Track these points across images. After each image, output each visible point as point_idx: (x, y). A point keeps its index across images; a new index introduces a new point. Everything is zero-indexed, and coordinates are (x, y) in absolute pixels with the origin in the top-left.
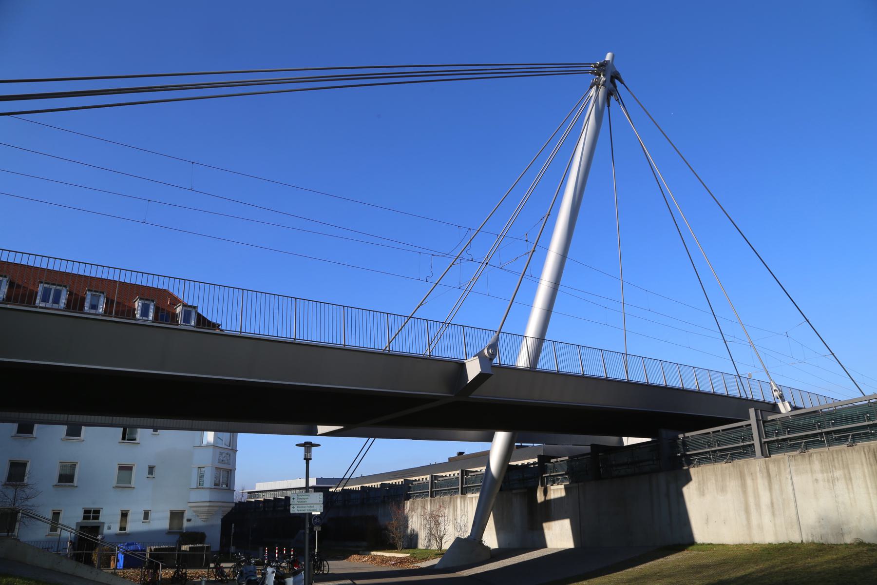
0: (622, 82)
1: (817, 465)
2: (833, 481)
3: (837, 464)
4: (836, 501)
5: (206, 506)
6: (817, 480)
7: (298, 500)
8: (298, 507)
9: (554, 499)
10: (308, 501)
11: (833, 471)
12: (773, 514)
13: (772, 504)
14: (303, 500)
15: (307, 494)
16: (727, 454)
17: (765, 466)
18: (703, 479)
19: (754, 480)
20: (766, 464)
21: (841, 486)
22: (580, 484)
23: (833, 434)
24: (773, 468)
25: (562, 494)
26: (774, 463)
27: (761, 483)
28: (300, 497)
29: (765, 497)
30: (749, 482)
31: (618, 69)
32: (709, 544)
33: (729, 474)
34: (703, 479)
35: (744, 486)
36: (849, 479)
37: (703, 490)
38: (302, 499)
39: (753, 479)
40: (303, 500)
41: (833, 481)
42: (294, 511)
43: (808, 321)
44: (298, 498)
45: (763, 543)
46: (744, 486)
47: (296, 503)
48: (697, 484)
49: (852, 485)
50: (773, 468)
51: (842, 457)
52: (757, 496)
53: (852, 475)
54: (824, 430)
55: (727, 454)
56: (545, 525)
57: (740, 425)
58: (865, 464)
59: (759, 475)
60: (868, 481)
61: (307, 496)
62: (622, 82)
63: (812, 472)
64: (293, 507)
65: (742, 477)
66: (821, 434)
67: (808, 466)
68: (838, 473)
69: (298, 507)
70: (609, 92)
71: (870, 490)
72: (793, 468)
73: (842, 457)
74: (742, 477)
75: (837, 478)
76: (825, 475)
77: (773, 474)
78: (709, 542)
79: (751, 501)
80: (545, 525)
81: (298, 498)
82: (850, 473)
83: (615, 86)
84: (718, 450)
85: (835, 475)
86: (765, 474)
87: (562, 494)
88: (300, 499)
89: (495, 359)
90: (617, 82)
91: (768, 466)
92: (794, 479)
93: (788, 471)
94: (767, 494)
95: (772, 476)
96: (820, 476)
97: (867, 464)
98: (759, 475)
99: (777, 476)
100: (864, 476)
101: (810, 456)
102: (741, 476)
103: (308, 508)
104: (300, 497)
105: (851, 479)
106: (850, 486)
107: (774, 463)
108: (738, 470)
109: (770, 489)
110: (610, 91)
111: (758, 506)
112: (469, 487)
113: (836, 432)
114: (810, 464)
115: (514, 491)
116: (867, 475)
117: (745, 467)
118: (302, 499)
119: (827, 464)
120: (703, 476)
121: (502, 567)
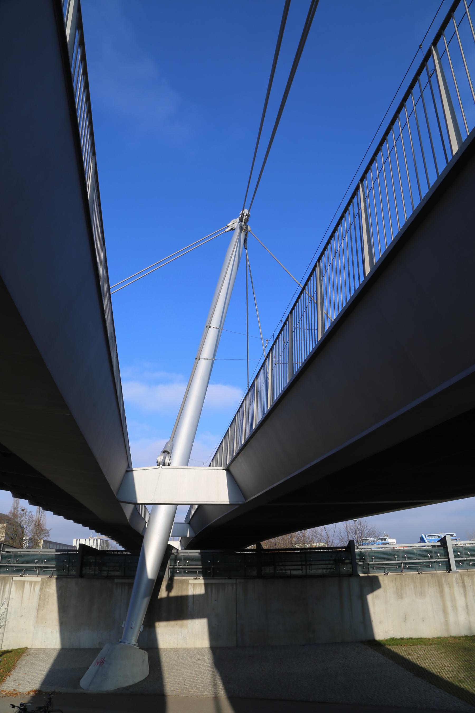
5: (212, 590)
9: (194, 596)
12: (468, 614)
13: (467, 607)
16: (23, 570)
17: (460, 579)
18: (401, 585)
19: (451, 587)
20: (461, 577)
23: (43, 568)
25: (201, 590)
26: (469, 577)
27: (458, 591)
29: (461, 602)
30: (446, 589)
32: (409, 638)
33: (428, 582)
34: (401, 585)
35: (442, 593)
37: (402, 594)
39: (450, 587)
46: (442, 593)
48: (395, 589)
52: (454, 600)
54: (38, 565)
55: (23, 570)
56: (142, 631)
59: (455, 584)
65: (440, 585)
66: (36, 567)
74: (440, 585)
77: (467, 584)
78: (408, 637)
79: (449, 604)
80: (142, 631)
84: (15, 566)
86: (461, 584)
87: (201, 590)
91: (463, 578)
95: (466, 586)
98: (455, 584)
99: (471, 586)
102: (439, 585)
107: (469, 577)
108: (436, 580)
109: (465, 595)
111: (455, 608)
112: (12, 566)
113: (16, 567)
117: (443, 578)
120: (401, 583)
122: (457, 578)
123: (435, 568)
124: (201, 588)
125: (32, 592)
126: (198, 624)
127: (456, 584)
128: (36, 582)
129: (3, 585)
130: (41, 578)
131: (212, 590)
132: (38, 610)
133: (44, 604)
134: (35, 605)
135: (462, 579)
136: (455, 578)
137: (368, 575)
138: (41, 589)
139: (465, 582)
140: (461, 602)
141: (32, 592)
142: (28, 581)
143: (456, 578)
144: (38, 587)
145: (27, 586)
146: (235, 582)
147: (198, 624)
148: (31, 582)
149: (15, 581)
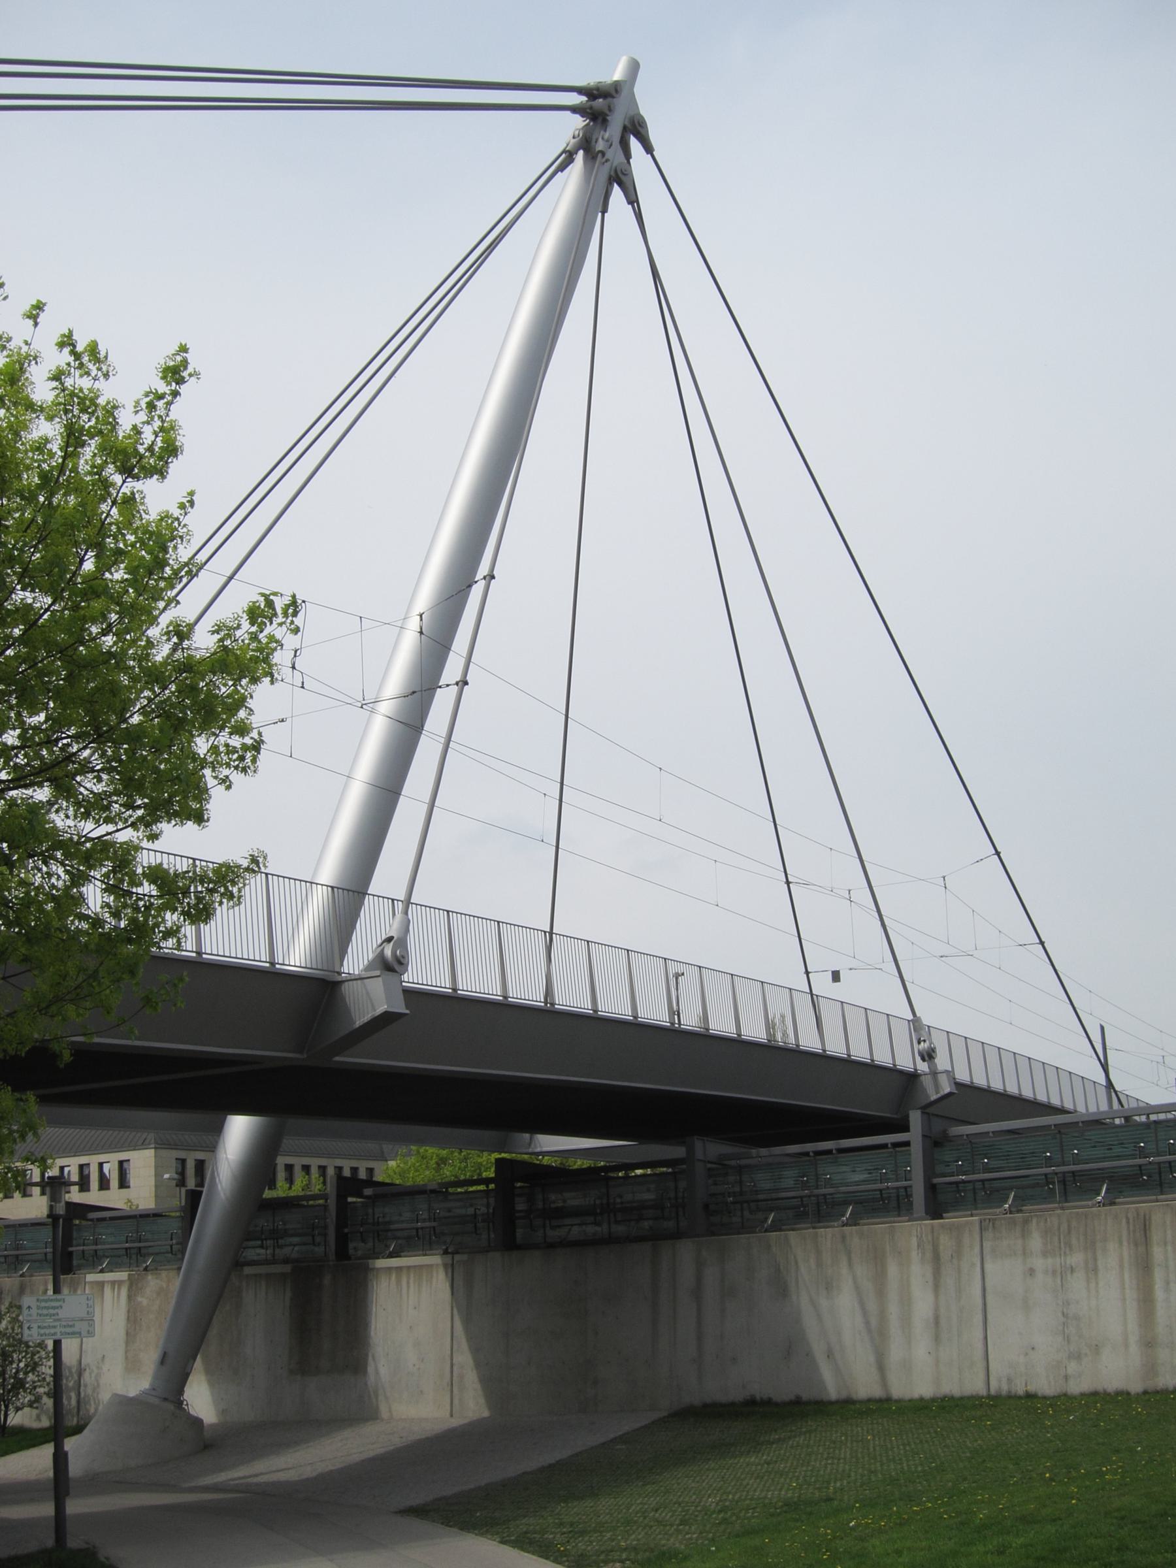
0: (648, 149)
1: (1036, 1242)
2: (1062, 1273)
3: (1074, 1241)
4: (1063, 1313)
5: (408, 1283)
6: (1032, 1272)
7: (40, 1312)
8: (39, 1327)
10: (62, 1314)
11: (1065, 1253)
12: (937, 1339)
14: (52, 1311)
15: (58, 1297)
17: (930, 1238)
20: (933, 1232)
21: (1077, 1282)
22: (457, 1257)
24: (946, 1243)
27: (919, 1272)
28: (43, 1304)
29: (923, 1304)
30: (893, 1270)
31: (646, 110)
36: (1092, 1270)
38: (48, 1308)
40: (52, 1311)
41: (1062, 1273)
42: (31, 1336)
43: (998, 853)
44: (38, 1308)
45: (907, 1396)
47: (35, 1317)
49: (1097, 1283)
50: (946, 1243)
51: (1086, 1226)
52: (906, 1301)
53: (1099, 1263)
57: (883, 1142)
58: (1125, 1243)
60: (1127, 1276)
61: (59, 1300)
62: (648, 149)
63: (1024, 1253)
64: (29, 1328)
67: (1020, 1242)
68: (1077, 1258)
69: (39, 1327)
70: (613, 173)
71: (1127, 1291)
72: (987, 1245)
73: (1086, 1226)
75: (1072, 1267)
76: (1058, 1259)
77: (945, 1254)
81: (38, 1308)
82: (1095, 1260)
83: (628, 155)
85: (1068, 1262)
86: (929, 1255)
88: (45, 1307)
89: (406, 975)
90: (635, 144)
92: (989, 1266)
93: (977, 1249)
94: (930, 1297)
96: (1039, 1263)
97: (1129, 1243)
98: (915, 1255)
100: (1121, 1266)
101: (1026, 1222)
103: (63, 1330)
104: (43, 1304)
105: (1095, 1270)
106: (1093, 1285)
109: (936, 1287)
110: (616, 171)
114: (1023, 1236)
115: (248, 1270)
116: (1126, 1265)
118: (48, 1308)
119: (1056, 1239)
121: (356, 1459)
122: (922, 1236)
123: (1077, 1178)
124: (390, 1279)
125: (115, 1304)
126: (836, 976)
127: (918, 1253)
128: (120, 1283)
129: (116, 1290)
130: (129, 1274)
131: (408, 1283)
132: (127, 1343)
133: (135, 1329)
134: (123, 1333)
135: (933, 1239)
136: (917, 1236)
137: (163, 599)
138: (130, 1298)
139: (941, 1247)
140: (923, 1304)
141: (115, 1304)
142: (108, 1282)
143: (919, 1236)
144: (124, 1292)
145: (108, 1290)
146: (451, 1262)
147: (836, 976)
148: (113, 1283)
149: (91, 1283)
